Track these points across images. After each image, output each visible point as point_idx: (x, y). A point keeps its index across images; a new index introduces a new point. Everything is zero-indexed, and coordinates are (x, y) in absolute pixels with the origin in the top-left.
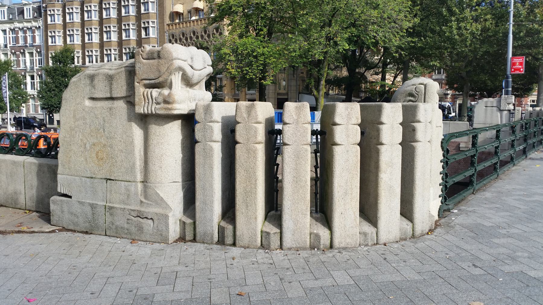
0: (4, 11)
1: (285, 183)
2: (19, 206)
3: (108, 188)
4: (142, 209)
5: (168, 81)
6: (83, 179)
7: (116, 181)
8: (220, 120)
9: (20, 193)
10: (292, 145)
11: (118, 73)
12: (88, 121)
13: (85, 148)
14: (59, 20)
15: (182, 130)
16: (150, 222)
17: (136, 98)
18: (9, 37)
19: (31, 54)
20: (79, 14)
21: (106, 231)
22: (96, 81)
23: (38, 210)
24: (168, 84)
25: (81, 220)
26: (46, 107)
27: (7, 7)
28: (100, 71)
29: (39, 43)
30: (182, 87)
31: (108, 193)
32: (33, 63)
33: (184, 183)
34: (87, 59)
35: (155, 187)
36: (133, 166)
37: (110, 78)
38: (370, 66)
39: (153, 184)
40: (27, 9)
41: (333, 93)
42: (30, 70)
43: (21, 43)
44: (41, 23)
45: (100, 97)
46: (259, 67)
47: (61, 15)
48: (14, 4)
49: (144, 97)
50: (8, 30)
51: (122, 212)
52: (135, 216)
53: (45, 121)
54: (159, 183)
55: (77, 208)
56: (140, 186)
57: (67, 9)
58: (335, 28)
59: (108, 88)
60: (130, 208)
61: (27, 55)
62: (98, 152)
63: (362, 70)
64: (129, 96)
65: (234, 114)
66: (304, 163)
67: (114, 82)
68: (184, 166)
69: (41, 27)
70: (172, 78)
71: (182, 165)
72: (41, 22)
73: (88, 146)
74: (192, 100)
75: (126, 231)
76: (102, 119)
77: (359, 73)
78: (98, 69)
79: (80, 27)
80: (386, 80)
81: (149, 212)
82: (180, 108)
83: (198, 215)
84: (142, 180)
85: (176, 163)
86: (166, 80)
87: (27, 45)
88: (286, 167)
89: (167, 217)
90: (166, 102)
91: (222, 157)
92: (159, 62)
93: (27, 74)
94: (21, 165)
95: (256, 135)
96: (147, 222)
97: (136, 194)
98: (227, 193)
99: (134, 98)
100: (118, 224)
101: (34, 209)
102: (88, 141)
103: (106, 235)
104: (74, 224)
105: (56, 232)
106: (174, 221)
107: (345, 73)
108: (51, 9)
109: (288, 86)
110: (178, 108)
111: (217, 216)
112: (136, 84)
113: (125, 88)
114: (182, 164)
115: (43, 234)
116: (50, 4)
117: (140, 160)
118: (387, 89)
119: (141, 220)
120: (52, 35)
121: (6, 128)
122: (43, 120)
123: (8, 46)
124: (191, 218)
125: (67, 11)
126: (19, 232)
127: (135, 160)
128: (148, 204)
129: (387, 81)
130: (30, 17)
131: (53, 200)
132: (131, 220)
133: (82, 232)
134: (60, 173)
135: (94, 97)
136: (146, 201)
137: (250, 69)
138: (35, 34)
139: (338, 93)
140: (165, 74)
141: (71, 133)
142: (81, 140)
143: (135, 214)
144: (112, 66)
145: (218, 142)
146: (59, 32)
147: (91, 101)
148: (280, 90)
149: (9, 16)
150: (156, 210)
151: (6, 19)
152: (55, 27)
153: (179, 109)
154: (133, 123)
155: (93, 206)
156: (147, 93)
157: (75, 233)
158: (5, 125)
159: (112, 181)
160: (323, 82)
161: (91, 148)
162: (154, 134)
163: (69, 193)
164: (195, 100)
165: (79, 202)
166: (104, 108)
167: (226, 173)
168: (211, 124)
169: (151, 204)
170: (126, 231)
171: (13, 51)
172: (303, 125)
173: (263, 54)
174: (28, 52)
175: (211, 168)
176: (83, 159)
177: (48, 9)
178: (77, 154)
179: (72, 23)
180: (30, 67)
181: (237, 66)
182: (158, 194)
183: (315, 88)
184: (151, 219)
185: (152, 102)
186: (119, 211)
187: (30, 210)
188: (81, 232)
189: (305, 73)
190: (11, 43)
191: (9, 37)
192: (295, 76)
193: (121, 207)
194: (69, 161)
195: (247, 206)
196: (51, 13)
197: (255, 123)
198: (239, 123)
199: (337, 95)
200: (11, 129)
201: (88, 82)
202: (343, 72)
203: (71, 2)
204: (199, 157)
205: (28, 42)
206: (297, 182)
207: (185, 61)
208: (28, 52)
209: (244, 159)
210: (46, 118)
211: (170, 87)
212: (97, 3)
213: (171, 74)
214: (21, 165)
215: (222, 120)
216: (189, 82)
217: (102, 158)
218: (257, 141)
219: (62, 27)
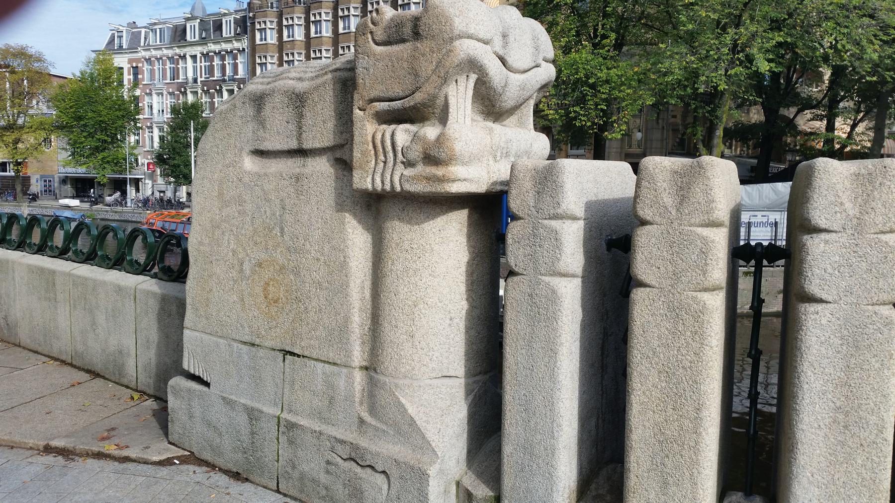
0: (194, 25)
1: (805, 427)
3: (287, 374)
4: (363, 443)
5: (438, 101)
6: (235, 345)
7: (306, 360)
8: (580, 212)
9: (129, 355)
10: (835, 302)
11: (317, 88)
12: (249, 207)
13: (241, 271)
14: (272, 38)
15: (469, 237)
16: (380, 479)
17: (355, 150)
18: (201, 67)
20: (303, 26)
21: (278, 480)
22: (267, 110)
23: (157, 394)
24: (437, 111)
25: (227, 444)
27: (199, 21)
28: (276, 84)
29: (243, 75)
30: (475, 118)
31: (286, 386)
33: (471, 380)
35: (396, 386)
36: (344, 327)
37: (298, 101)
38: (807, 104)
39: (392, 380)
40: (227, 21)
41: (731, 153)
43: (217, 75)
44: (246, 44)
45: (275, 149)
46: (600, 105)
47: (275, 30)
48: (209, 15)
49: (375, 147)
50: (199, 55)
51: (315, 441)
52: (345, 457)
54: (405, 377)
55: (220, 415)
56: (359, 377)
57: (284, 20)
58: (749, 28)
59: (292, 127)
60: (334, 434)
62: (268, 284)
63: (791, 112)
64: (340, 146)
65: (630, 193)
66: (877, 365)
67: (308, 113)
68: (473, 332)
69: (246, 50)
70: (450, 93)
71: (467, 332)
72: (246, 41)
73: (247, 267)
74: (499, 154)
75: (324, 492)
76: (277, 202)
77: (785, 118)
78: (274, 79)
79: (304, 48)
80: (836, 131)
81: (378, 454)
82: (466, 176)
83: (508, 481)
84: (364, 364)
85: (450, 325)
86: (434, 98)
87: (226, 78)
88: (809, 373)
89: (422, 477)
90: (430, 159)
91: (583, 321)
92: (416, 49)
95: (706, 264)
96: (372, 479)
97: (349, 398)
98: (593, 422)
99: (351, 150)
100: (306, 469)
101: (151, 391)
102: (247, 255)
103: (278, 491)
104: (213, 450)
105: (175, 463)
106: (442, 489)
107: (756, 115)
108: (261, 20)
109: (646, 141)
110: (463, 177)
111: (566, 496)
112: (357, 112)
113: (331, 125)
114: (468, 329)
115: (146, 466)
116: (260, 13)
117: (360, 310)
118: (837, 146)
119: (358, 470)
120: (262, 62)
123: (199, 80)
124: (487, 483)
125: (285, 23)
126: (99, 456)
127: (349, 311)
128: (377, 429)
129: (836, 133)
130: (230, 33)
131: (172, 387)
132: (336, 465)
133: (227, 472)
134: (189, 326)
135: (262, 148)
136: (374, 423)
137: (581, 108)
138: (237, 61)
139: (741, 154)
140: (431, 80)
141: (213, 234)
142: (234, 251)
143: (345, 452)
144: (306, 72)
145: (574, 276)
146: (272, 57)
147: (257, 159)
148: (630, 147)
149: (200, 34)
150: (397, 448)
151: (197, 38)
152: (267, 48)
153: (465, 180)
154: (347, 215)
155: (253, 415)
156: (383, 135)
157: (212, 474)
159: (296, 358)
160: (720, 132)
161: (253, 272)
162: (397, 244)
163: (205, 374)
164: (507, 155)
165: (224, 399)
166: (284, 175)
167: (592, 365)
168: (554, 223)
169: (384, 431)
170: (324, 492)
171: (205, 88)
172: (881, 236)
173: (607, 82)
174: (227, 90)
175: (552, 352)
176: (235, 299)
177: (257, 21)
178: (225, 286)
179: (291, 43)
181: (558, 103)
182: (403, 406)
183: (703, 141)
184: (384, 472)
185: (395, 160)
186: (308, 438)
187: (143, 393)
188: (227, 471)
189: (679, 117)
190: (203, 75)
191: (201, 67)
192: (660, 121)
193: (312, 427)
194: (208, 299)
195: (666, 484)
196: (260, 26)
197: (702, 226)
198: (644, 223)
199: (739, 157)
201: (251, 111)
202: (751, 115)
203: (291, 8)
204: (516, 316)
205: (227, 74)
206: (846, 427)
207: (486, 42)
208: (226, 90)
209: (659, 337)
211: (443, 119)
212: (330, 8)
213: (445, 81)
215: (586, 211)
216: (494, 106)
217: (275, 298)
218: (707, 284)
219: (277, 49)
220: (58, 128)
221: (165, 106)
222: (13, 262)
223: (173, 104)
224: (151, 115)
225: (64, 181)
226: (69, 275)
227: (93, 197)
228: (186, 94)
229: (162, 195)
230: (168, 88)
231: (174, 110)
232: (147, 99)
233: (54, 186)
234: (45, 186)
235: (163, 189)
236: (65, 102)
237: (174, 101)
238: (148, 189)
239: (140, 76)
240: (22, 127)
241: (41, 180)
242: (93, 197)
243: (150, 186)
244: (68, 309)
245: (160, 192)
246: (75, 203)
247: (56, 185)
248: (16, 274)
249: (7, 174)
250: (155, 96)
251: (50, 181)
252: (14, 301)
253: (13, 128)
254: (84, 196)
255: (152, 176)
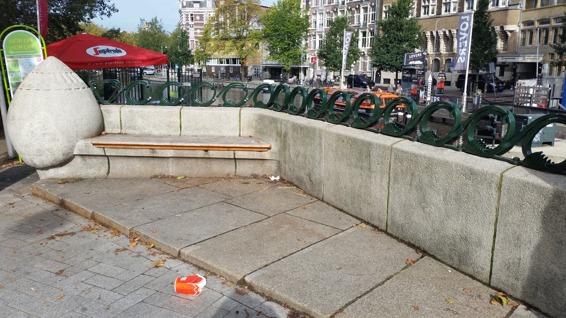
2: (470, 270)
9: (479, 244)
19: (366, 9)
26: (378, 64)
32: (367, 19)
34: (422, 10)
42: (363, 26)
53: (372, 79)
61: (362, 10)
93: (360, 31)
94: (492, 182)
101: (518, 295)
121: (338, 85)
122: (371, 78)
158: (338, 83)
180: (363, 23)
200: (344, 87)
210: (373, 76)
214: (492, 182)
220: (265, 37)
221: (324, 21)
222: (321, 131)
223: (329, 19)
224: (315, 28)
225: (265, 69)
226: (391, 149)
227: (282, 79)
228: (337, 12)
229: (319, 77)
230: (326, 9)
231: (330, 23)
232: (313, 17)
233: (260, 72)
234: (255, 72)
235: (320, 74)
236: (269, 21)
237: (329, 17)
238: (310, 74)
239: (310, 3)
240: (245, 38)
241: (253, 69)
242: (282, 79)
243: (312, 72)
244: (386, 180)
245: (318, 76)
246: (271, 82)
247: (261, 71)
248: (323, 140)
249: (236, 65)
250: (318, 15)
251: (258, 69)
252: (320, 163)
253: (241, 38)
254: (276, 78)
255: (313, 66)
